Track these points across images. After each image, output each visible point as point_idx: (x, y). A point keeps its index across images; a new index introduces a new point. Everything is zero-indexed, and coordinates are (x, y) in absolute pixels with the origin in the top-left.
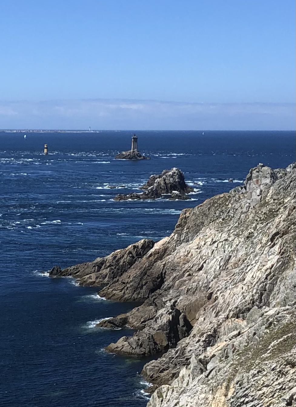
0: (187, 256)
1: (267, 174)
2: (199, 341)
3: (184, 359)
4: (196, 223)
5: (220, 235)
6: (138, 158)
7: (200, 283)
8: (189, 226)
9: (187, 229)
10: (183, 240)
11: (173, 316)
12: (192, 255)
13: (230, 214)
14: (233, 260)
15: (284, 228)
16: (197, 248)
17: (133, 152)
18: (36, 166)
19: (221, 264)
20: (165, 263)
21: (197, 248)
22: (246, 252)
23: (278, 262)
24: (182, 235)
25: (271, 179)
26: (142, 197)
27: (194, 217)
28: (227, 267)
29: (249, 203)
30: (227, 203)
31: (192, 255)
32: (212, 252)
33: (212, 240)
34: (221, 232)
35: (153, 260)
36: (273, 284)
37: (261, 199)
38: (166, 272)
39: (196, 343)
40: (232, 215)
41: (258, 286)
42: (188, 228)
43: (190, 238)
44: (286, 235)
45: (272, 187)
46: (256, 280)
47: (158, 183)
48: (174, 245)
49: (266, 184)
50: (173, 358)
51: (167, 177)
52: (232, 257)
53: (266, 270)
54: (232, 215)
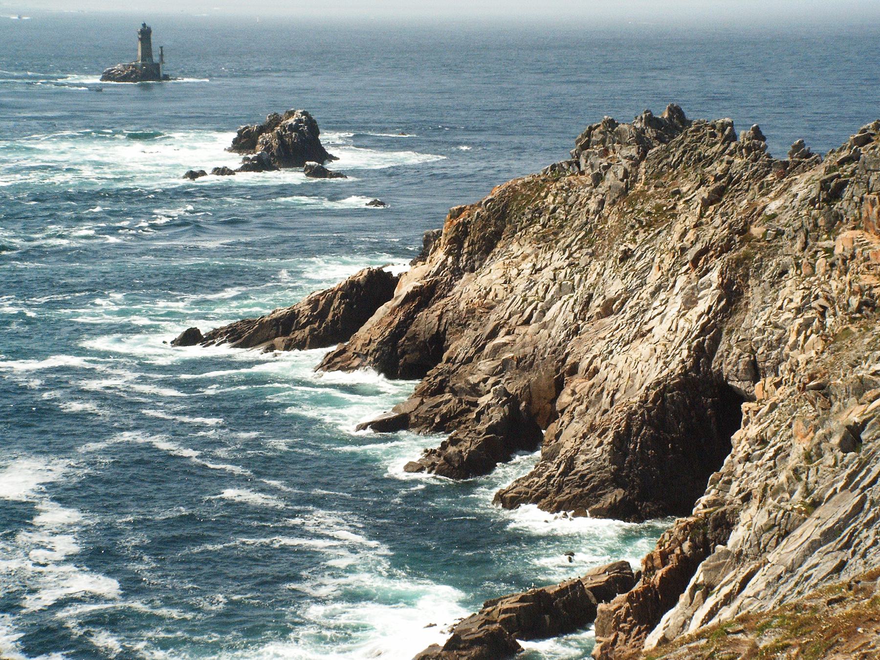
0: (485, 297)
2: (601, 444)
3: (577, 477)
5: (548, 256)
7: (540, 347)
9: (469, 246)
10: (464, 267)
11: (509, 407)
12: (496, 296)
14: (597, 302)
15: (723, 240)
16: (505, 283)
18: (465, 138)
19: (576, 311)
20: (442, 313)
21: (505, 283)
22: (624, 286)
23: (719, 300)
27: (480, 224)
28: (588, 316)
29: (603, 195)
30: (543, 194)
31: (496, 296)
32: (547, 288)
33: (534, 265)
34: (549, 249)
36: (716, 341)
37: (627, 186)
39: (596, 447)
40: (564, 217)
41: (689, 343)
43: (477, 264)
44: (727, 252)
45: (643, 164)
46: (681, 335)
47: (267, 143)
48: (449, 276)
49: (631, 158)
50: (554, 476)
51: (285, 130)
52: (595, 297)
53: (700, 316)
54: (564, 217)
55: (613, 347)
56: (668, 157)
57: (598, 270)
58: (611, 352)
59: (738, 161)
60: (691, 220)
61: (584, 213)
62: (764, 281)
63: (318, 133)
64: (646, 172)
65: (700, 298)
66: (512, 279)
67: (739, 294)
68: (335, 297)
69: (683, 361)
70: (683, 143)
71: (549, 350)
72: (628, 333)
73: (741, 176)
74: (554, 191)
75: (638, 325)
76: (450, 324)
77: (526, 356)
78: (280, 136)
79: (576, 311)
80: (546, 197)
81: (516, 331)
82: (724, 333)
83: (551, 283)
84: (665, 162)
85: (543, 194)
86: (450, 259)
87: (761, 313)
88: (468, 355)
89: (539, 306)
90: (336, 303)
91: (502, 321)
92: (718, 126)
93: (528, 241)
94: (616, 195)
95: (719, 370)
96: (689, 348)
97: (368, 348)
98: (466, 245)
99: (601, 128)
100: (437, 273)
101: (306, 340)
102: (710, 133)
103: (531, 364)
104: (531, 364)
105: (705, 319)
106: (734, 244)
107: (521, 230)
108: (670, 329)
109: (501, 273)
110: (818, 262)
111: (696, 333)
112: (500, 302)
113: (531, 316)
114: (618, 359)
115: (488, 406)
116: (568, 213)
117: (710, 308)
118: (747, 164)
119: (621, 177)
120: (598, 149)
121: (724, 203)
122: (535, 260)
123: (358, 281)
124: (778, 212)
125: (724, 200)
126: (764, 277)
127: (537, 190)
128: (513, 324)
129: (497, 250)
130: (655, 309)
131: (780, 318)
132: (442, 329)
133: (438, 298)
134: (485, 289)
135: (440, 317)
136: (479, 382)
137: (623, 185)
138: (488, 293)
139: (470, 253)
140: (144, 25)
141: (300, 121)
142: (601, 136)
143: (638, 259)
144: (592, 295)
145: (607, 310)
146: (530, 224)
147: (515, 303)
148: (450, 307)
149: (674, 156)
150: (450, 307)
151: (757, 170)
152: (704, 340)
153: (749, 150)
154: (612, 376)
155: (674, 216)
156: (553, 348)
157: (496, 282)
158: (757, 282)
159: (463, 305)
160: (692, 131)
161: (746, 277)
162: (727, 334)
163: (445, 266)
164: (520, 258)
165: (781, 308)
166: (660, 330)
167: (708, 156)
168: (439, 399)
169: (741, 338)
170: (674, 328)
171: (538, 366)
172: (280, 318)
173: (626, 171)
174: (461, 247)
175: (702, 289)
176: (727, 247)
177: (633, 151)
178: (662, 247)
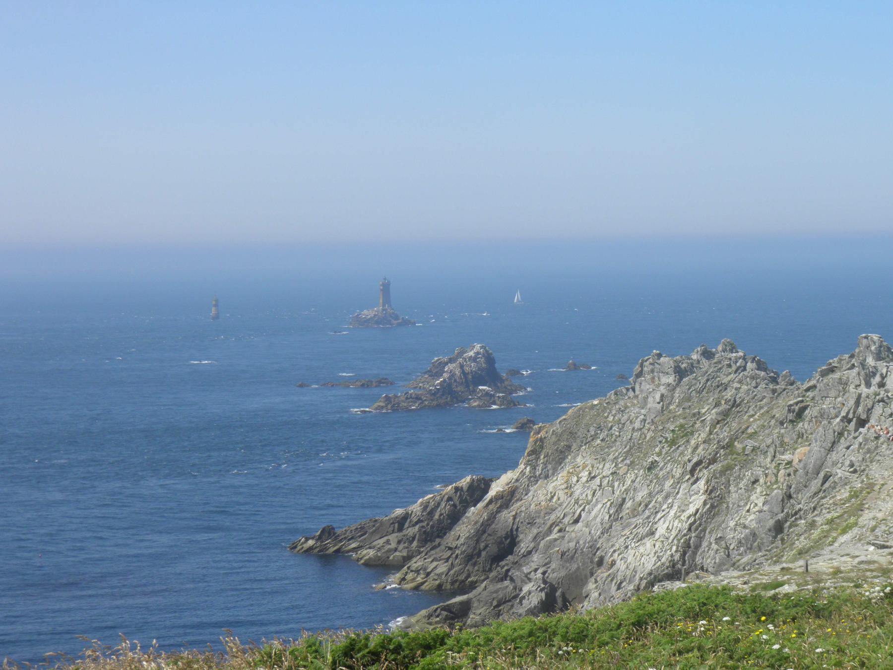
0: (551, 500)
1: (669, 368)
4: (558, 448)
5: (601, 467)
6: (393, 321)
7: (581, 542)
8: (548, 453)
9: (544, 458)
12: (559, 499)
13: (613, 432)
14: (629, 504)
17: (383, 310)
21: (566, 488)
22: (649, 492)
23: (705, 503)
24: (537, 468)
25: (675, 377)
26: (425, 398)
27: (554, 439)
29: (645, 415)
30: (606, 415)
32: (594, 493)
33: (590, 473)
35: (495, 509)
36: (700, 538)
37: (662, 408)
38: (518, 528)
42: (547, 456)
43: (551, 472)
44: (713, 464)
45: (678, 390)
46: (674, 533)
48: (527, 483)
51: (465, 361)
52: (627, 500)
53: (689, 518)
55: (629, 543)
56: (695, 384)
57: (632, 478)
58: (627, 547)
59: (745, 387)
60: (703, 436)
61: (631, 430)
62: (741, 488)
63: (495, 363)
64: (679, 396)
65: (691, 503)
66: (573, 485)
67: (722, 498)
68: (442, 500)
69: (672, 556)
70: (707, 372)
71: (587, 545)
72: (642, 531)
73: (743, 400)
74: (614, 412)
75: (651, 524)
76: (522, 523)
77: (569, 549)
78: (462, 366)
79: (611, 512)
80: (608, 417)
81: (567, 529)
82: (707, 532)
83: (598, 488)
84: (693, 388)
85: (606, 415)
86: (528, 469)
87: (736, 515)
88: (529, 549)
89: (586, 507)
90: (443, 504)
91: (558, 520)
92: (733, 359)
93: (589, 453)
94: (654, 416)
95: (702, 563)
96: (678, 546)
97: (457, 542)
98: (542, 457)
99: (651, 360)
100: (517, 480)
101: (416, 535)
102: (727, 365)
103: (572, 558)
104: (572, 558)
105: (692, 519)
106: (720, 457)
107: (585, 444)
108: (668, 528)
109: (565, 480)
110: (780, 472)
111: (685, 532)
112: (560, 505)
113: (580, 516)
114: (630, 555)
115: (530, 592)
116: (620, 430)
117: (697, 511)
118: (749, 390)
119: (658, 400)
120: (648, 377)
121: (727, 423)
122: (591, 469)
123: (462, 488)
124: (758, 430)
125: (728, 420)
126: (741, 485)
127: (602, 411)
128: (566, 523)
129: (567, 460)
130: (663, 511)
131: (746, 520)
132: (515, 527)
133: (517, 500)
134: (551, 493)
135: (515, 517)
136: (531, 572)
137: (659, 406)
138: (552, 497)
139: (545, 464)
140: (385, 279)
141: (478, 353)
142: (651, 367)
143: (661, 469)
144: (625, 499)
145: (634, 513)
146: (593, 440)
147: (569, 505)
148: (523, 509)
149: (700, 383)
150: (523, 509)
151: (756, 395)
152: (690, 538)
153: (753, 378)
154: (623, 567)
155: (692, 433)
156: (591, 544)
157: (560, 487)
158: (736, 489)
159: (533, 506)
160: (716, 363)
161: (728, 484)
162: (709, 533)
163: (524, 474)
164: (581, 468)
165: (748, 511)
166: (661, 529)
167: (724, 384)
168: (499, 586)
169: (719, 536)
170: (670, 527)
171: (577, 559)
172: (397, 518)
173: (662, 396)
174: (538, 458)
175: (693, 495)
176: (713, 461)
177: (671, 379)
178: (680, 459)
